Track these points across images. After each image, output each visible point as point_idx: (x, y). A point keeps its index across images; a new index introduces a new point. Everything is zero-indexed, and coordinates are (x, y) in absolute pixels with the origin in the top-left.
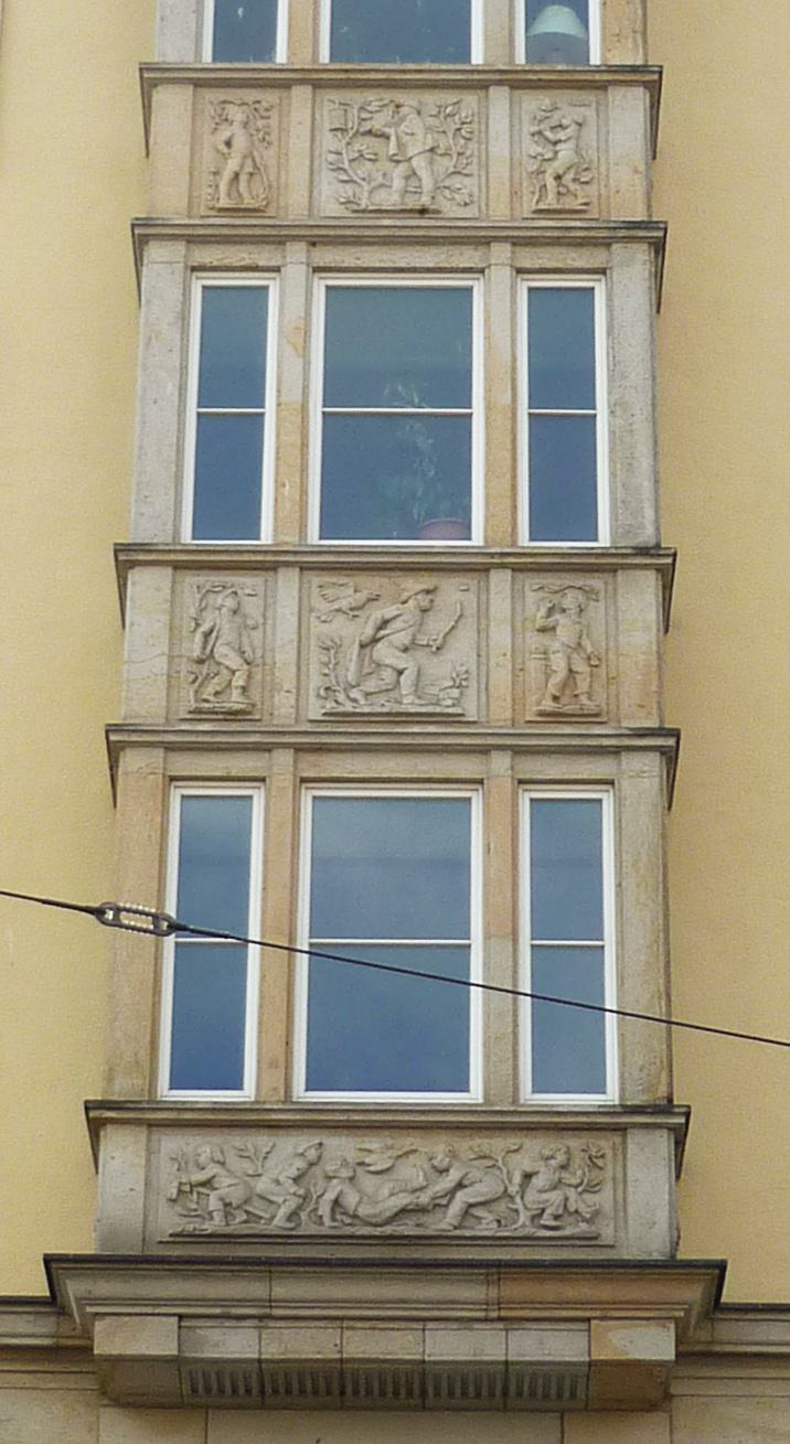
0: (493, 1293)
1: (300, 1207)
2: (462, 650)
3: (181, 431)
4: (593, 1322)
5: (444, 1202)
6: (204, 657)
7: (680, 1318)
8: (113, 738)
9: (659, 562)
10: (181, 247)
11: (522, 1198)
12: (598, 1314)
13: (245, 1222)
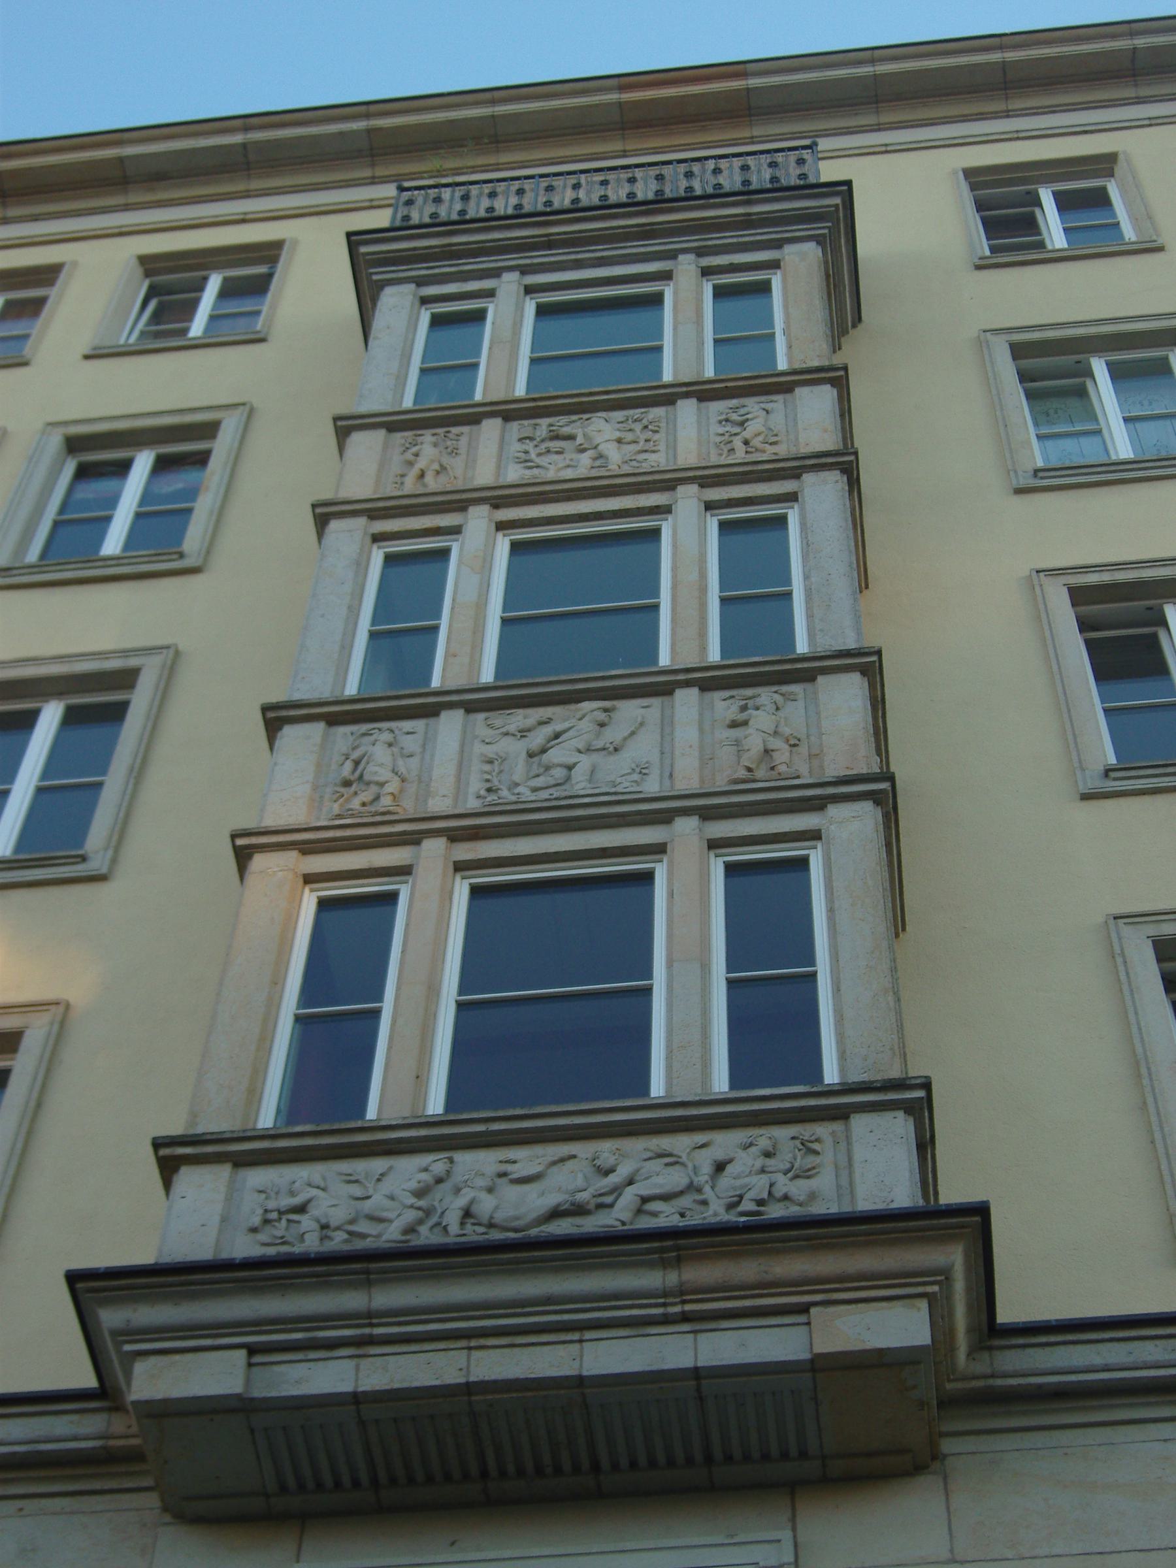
0: (672, 1278)
1: (421, 1222)
2: (644, 748)
3: (346, 648)
4: (813, 1310)
5: (608, 1200)
6: (352, 778)
7: (934, 1293)
8: (240, 842)
9: (867, 664)
10: (362, 521)
11: (712, 1188)
12: (818, 1298)
13: (346, 1241)
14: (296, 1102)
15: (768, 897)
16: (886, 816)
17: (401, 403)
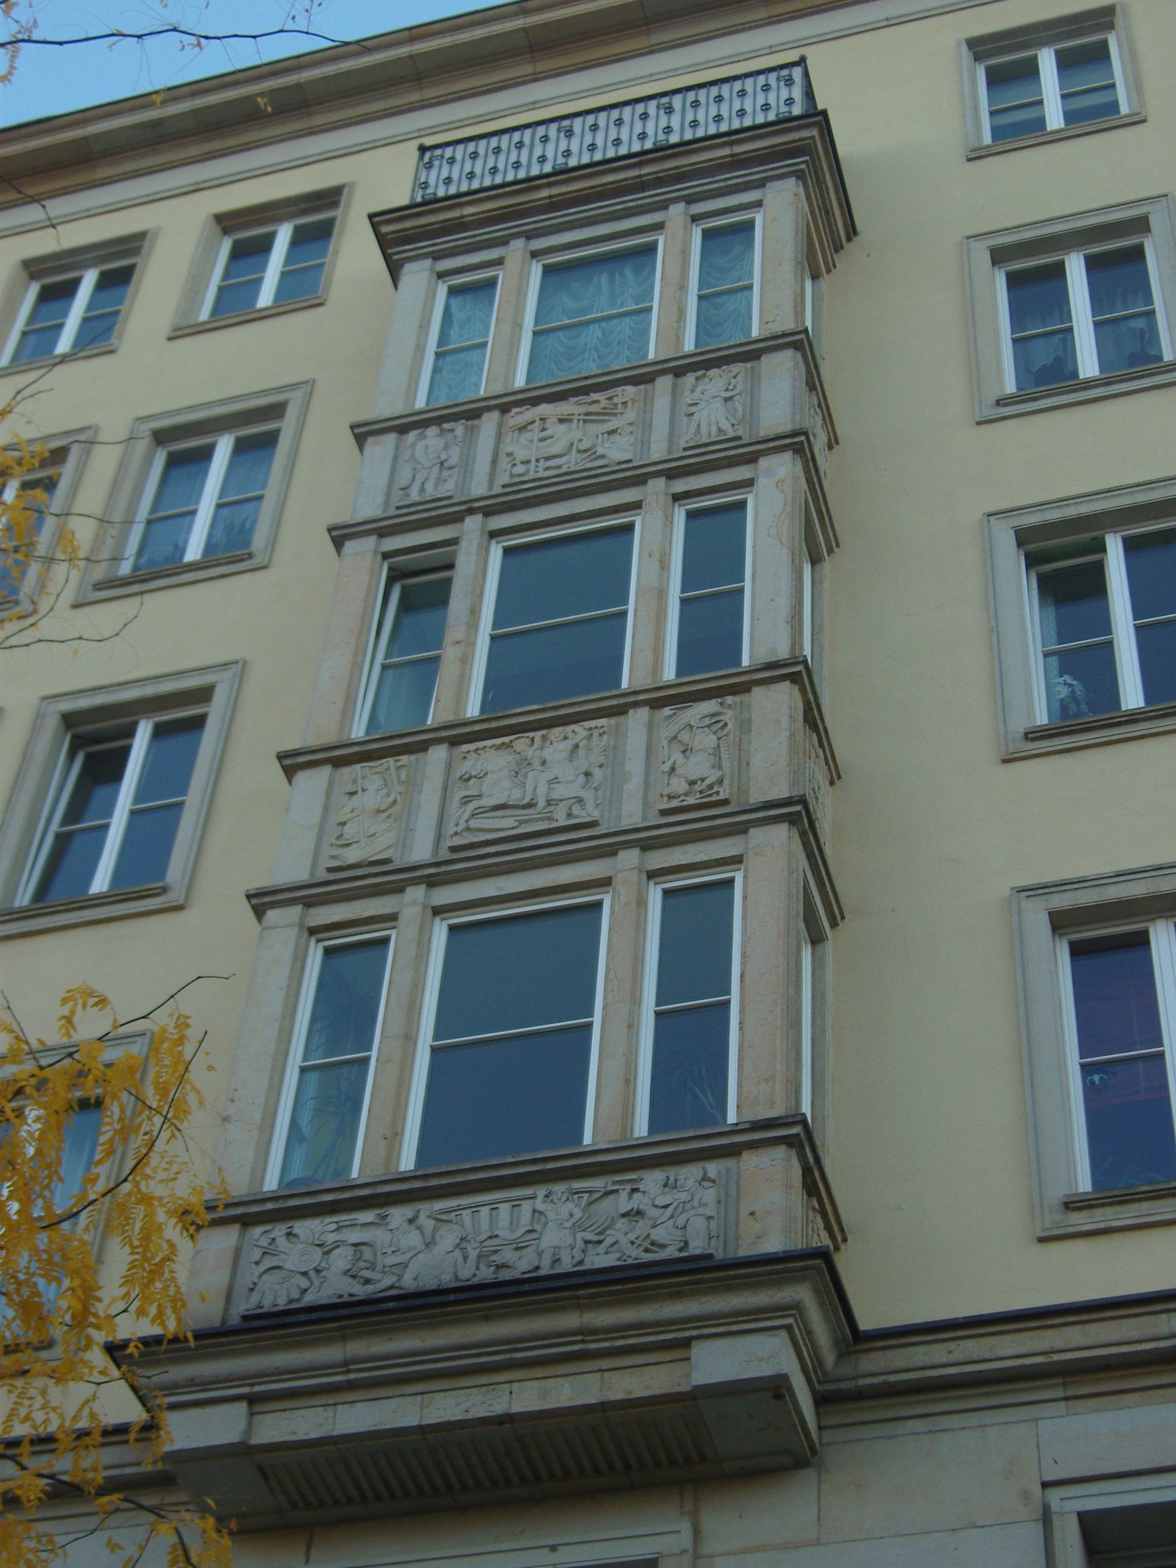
12: (694, 1333)
14: (691, 654)
15: (697, 919)
16: (803, 834)
17: (413, 405)
